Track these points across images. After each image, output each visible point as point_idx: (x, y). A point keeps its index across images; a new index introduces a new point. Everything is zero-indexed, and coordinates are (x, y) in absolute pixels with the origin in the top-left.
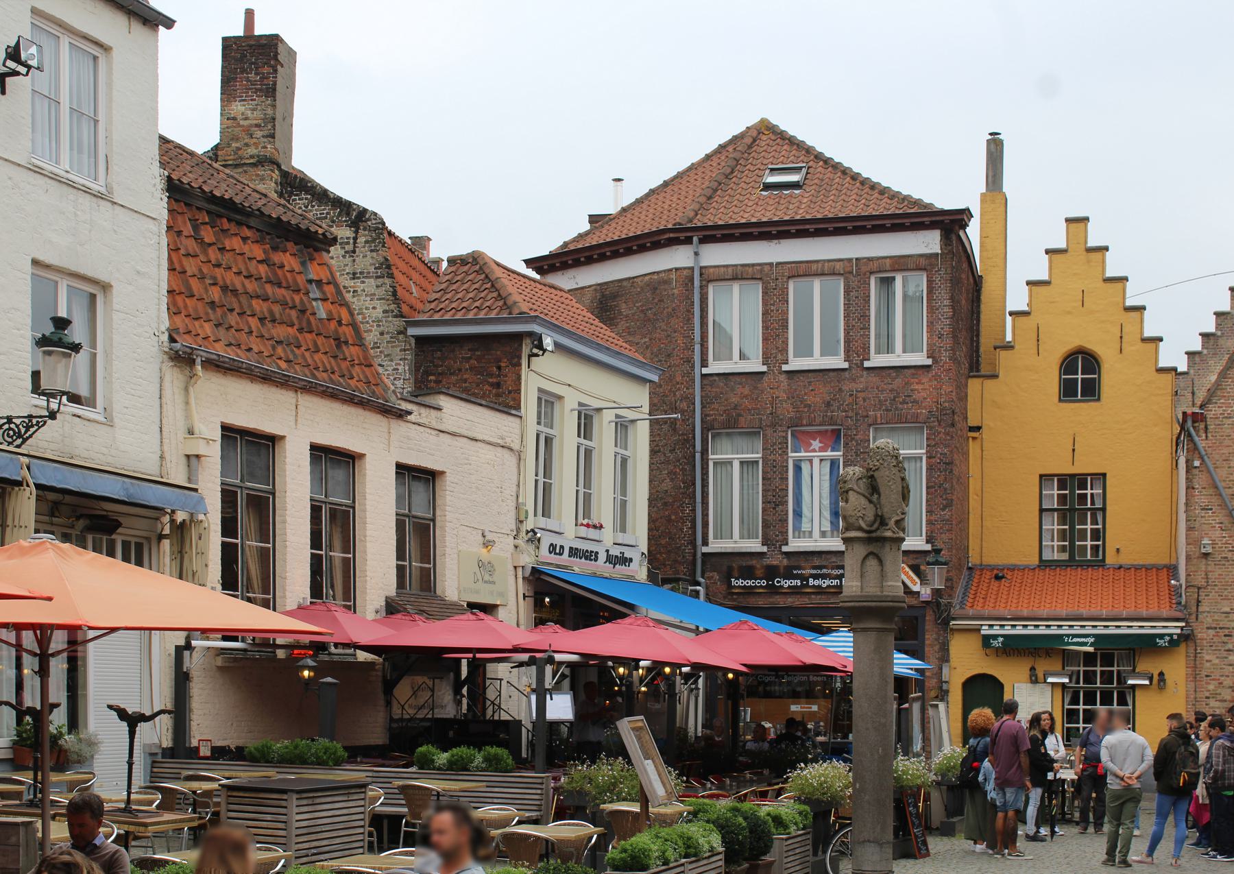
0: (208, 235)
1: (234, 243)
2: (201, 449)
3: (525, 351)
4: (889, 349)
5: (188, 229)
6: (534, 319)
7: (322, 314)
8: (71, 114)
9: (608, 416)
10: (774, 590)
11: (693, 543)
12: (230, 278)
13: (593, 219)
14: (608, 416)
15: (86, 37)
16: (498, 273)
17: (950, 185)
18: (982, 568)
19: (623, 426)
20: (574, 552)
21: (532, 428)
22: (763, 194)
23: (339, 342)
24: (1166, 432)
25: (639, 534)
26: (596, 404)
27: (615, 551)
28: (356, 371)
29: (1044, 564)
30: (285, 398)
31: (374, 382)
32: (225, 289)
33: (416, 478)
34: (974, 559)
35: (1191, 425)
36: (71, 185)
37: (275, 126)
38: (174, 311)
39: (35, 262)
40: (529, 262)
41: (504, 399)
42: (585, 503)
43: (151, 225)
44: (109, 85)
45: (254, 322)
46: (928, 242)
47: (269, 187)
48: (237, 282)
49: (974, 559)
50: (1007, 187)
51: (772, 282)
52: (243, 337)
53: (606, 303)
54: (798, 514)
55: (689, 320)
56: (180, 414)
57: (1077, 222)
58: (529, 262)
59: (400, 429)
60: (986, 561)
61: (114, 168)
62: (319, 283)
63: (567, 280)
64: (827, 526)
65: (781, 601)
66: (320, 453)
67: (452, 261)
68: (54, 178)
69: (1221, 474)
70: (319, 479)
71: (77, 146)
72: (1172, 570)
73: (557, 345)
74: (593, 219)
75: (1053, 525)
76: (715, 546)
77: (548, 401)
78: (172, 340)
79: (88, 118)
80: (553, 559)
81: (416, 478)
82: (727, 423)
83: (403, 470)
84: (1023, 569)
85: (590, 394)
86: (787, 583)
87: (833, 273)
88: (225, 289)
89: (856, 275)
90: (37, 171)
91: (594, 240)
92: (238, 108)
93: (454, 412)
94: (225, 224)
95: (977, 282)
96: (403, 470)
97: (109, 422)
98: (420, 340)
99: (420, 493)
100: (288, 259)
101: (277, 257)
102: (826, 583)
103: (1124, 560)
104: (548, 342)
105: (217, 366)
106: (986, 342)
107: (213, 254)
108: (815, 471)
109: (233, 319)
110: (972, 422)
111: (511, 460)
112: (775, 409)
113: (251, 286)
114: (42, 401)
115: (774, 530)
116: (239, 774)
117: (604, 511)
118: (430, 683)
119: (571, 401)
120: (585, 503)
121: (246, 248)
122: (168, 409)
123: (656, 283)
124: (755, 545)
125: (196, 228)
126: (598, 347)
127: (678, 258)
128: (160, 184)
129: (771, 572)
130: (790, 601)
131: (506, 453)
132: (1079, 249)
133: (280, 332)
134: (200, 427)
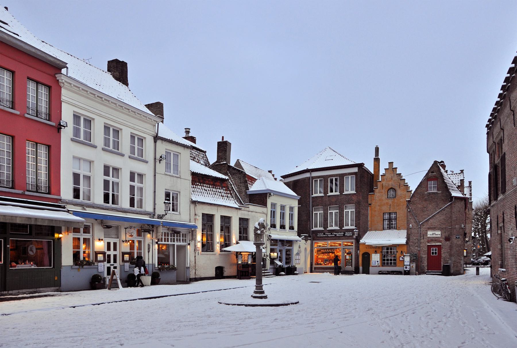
19: (291, 209)
36: (173, 176)
41: (265, 204)
43: (189, 181)
46: (356, 170)
55: (309, 187)
75: (84, 267)
77: (273, 205)
79: (176, 166)
92: (220, 154)
93: (252, 208)
97: (180, 214)
110: (369, 203)
116: (302, 255)
118: (354, 237)
123: (304, 180)
127: (307, 175)
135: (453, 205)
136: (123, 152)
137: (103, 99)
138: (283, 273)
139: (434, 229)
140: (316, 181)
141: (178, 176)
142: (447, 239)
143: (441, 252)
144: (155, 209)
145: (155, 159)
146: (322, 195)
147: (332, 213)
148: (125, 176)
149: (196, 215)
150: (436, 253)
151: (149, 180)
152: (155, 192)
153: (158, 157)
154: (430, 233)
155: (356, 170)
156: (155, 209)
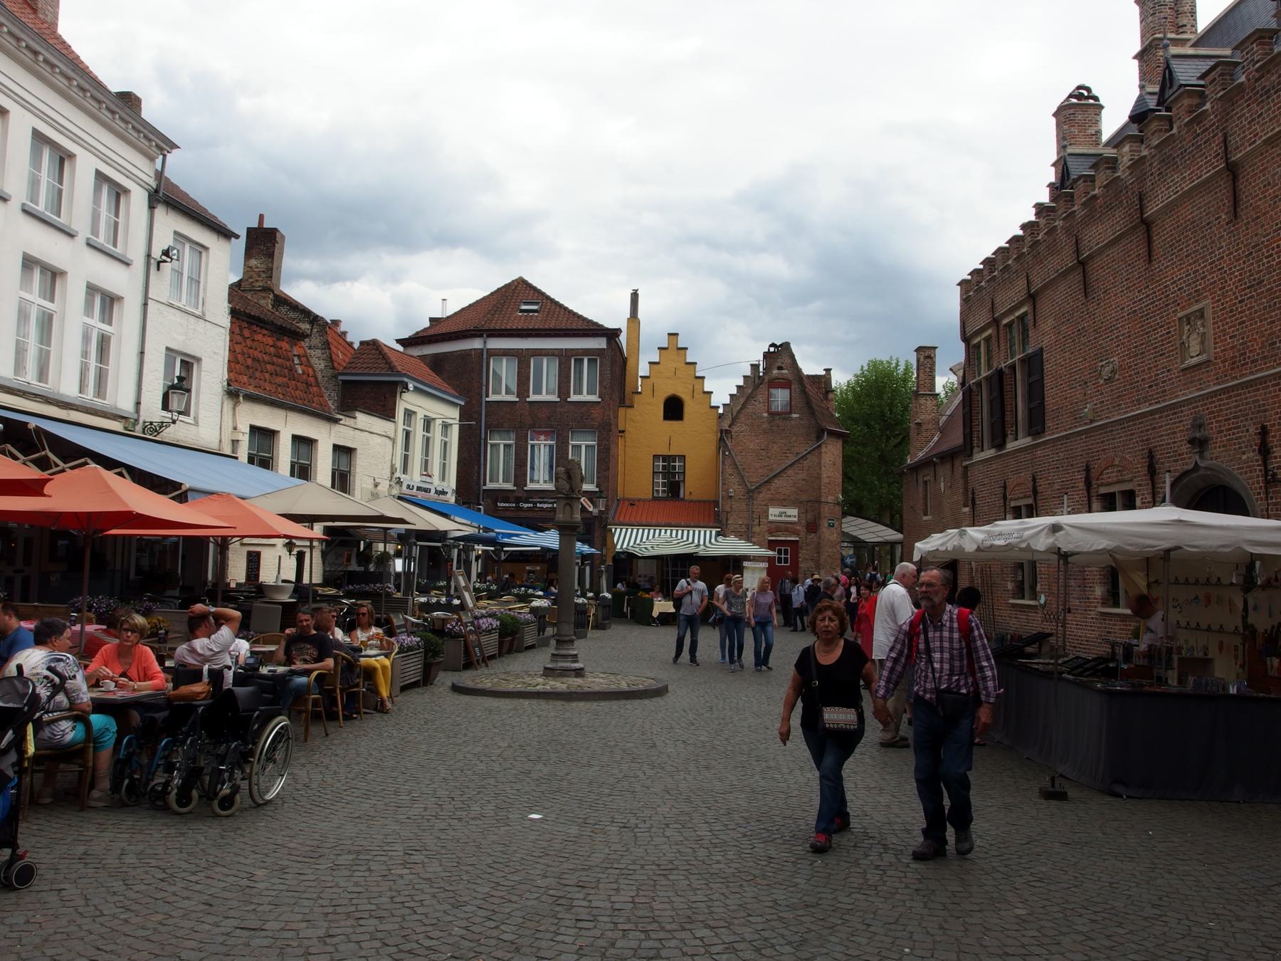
0: (246, 333)
1: (259, 337)
2: (240, 437)
3: (399, 390)
4: (580, 393)
5: (237, 331)
6: (405, 375)
7: (300, 371)
8: (97, 190)
9: (439, 422)
10: (519, 509)
11: (478, 484)
12: (257, 354)
13: (432, 320)
14: (439, 422)
15: (198, 244)
16: (386, 350)
17: (611, 314)
18: (624, 500)
19: (446, 426)
20: (419, 489)
21: (401, 426)
22: (517, 310)
23: (308, 385)
24: (713, 438)
25: (451, 483)
26: (433, 416)
27: (439, 489)
28: (316, 399)
29: (655, 499)
30: (280, 413)
31: (323, 405)
32: (254, 359)
33: (343, 452)
34: (620, 495)
35: (724, 436)
37: (271, 272)
38: (230, 370)
39: (168, 349)
40: (398, 341)
41: (387, 413)
42: (426, 464)
44: (207, 265)
45: (267, 375)
46: (600, 343)
47: (267, 303)
48: (260, 356)
49: (620, 495)
50: (640, 316)
51: (523, 358)
52: (262, 383)
53: (436, 363)
54: (532, 468)
56: (230, 421)
57: (673, 335)
58: (398, 341)
59: (337, 428)
60: (627, 496)
61: (207, 304)
62: (299, 356)
63: (416, 351)
64: (547, 478)
65: (522, 514)
66: (297, 439)
67: (362, 343)
68: (179, 309)
69: (737, 459)
70: (295, 451)
71: (189, 293)
72: (716, 503)
73: (415, 388)
74: (432, 320)
76: (490, 486)
78: (229, 385)
79: (195, 281)
80: (409, 492)
81: (343, 452)
82: (494, 427)
83: (337, 448)
84: (644, 501)
85: (431, 414)
86: (526, 506)
87: (553, 355)
88: (254, 359)
89: (564, 357)
90: (171, 306)
91: (432, 332)
92: (253, 262)
93: (362, 419)
94: (254, 327)
95: (625, 361)
96: (337, 448)
97: (196, 424)
98: (344, 382)
99: (344, 459)
100: (284, 345)
101: (279, 344)
102: (545, 506)
103: (693, 498)
104: (411, 386)
105: (250, 398)
106: (628, 390)
107: (249, 343)
108: (541, 450)
109: (258, 374)
110: (621, 428)
111: (390, 443)
112: (523, 419)
113: (266, 358)
114: (169, 415)
115: (520, 478)
117: (436, 469)
119: (420, 415)
120: (426, 464)
121: (265, 339)
122: (225, 417)
124: (509, 486)
125: (241, 330)
126: (435, 389)
127: (477, 344)
128: (227, 311)
129: (518, 500)
130: (530, 514)
131: (387, 440)
132: (674, 347)
133: (280, 380)
134: (240, 427)
135: (824, 449)
136: (75, 227)
137: (41, 58)
138: (541, 593)
139: (783, 503)
140: (579, 362)
141: (198, 312)
142: (812, 527)
143: (797, 557)
144: (138, 403)
145: (149, 256)
146: (513, 398)
147: (580, 446)
148: (74, 292)
149: (235, 428)
150: (786, 560)
151: (129, 313)
152: (142, 353)
153: (156, 253)
154: (774, 513)
155: (600, 343)
156: (138, 403)
